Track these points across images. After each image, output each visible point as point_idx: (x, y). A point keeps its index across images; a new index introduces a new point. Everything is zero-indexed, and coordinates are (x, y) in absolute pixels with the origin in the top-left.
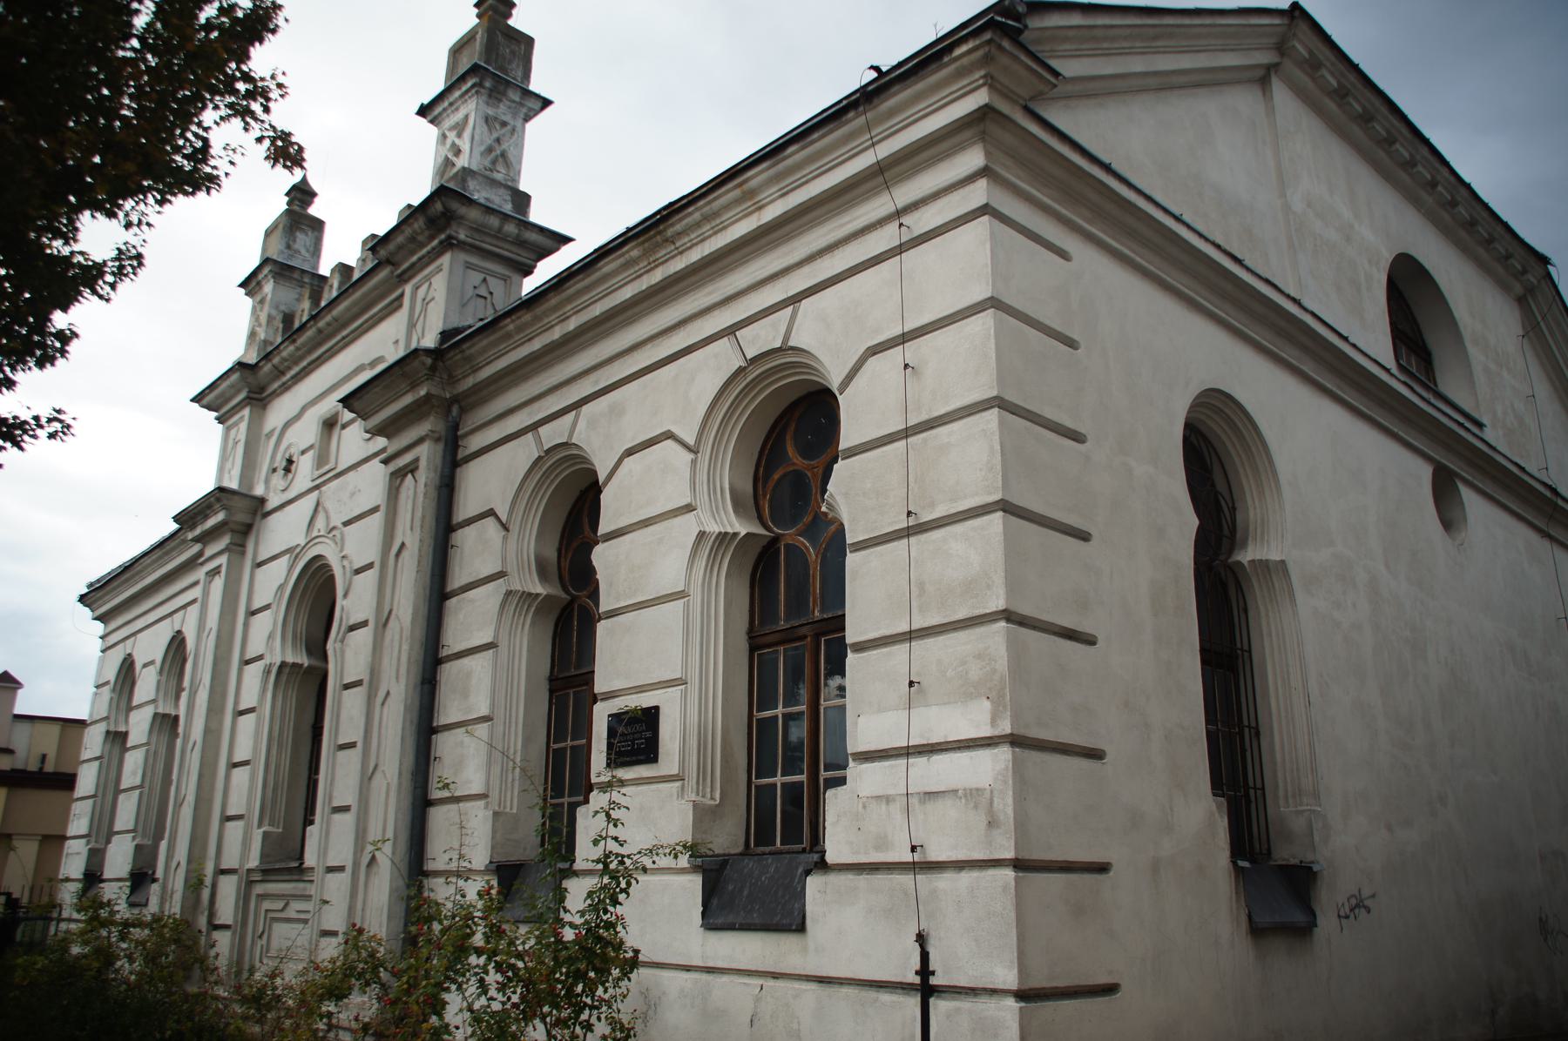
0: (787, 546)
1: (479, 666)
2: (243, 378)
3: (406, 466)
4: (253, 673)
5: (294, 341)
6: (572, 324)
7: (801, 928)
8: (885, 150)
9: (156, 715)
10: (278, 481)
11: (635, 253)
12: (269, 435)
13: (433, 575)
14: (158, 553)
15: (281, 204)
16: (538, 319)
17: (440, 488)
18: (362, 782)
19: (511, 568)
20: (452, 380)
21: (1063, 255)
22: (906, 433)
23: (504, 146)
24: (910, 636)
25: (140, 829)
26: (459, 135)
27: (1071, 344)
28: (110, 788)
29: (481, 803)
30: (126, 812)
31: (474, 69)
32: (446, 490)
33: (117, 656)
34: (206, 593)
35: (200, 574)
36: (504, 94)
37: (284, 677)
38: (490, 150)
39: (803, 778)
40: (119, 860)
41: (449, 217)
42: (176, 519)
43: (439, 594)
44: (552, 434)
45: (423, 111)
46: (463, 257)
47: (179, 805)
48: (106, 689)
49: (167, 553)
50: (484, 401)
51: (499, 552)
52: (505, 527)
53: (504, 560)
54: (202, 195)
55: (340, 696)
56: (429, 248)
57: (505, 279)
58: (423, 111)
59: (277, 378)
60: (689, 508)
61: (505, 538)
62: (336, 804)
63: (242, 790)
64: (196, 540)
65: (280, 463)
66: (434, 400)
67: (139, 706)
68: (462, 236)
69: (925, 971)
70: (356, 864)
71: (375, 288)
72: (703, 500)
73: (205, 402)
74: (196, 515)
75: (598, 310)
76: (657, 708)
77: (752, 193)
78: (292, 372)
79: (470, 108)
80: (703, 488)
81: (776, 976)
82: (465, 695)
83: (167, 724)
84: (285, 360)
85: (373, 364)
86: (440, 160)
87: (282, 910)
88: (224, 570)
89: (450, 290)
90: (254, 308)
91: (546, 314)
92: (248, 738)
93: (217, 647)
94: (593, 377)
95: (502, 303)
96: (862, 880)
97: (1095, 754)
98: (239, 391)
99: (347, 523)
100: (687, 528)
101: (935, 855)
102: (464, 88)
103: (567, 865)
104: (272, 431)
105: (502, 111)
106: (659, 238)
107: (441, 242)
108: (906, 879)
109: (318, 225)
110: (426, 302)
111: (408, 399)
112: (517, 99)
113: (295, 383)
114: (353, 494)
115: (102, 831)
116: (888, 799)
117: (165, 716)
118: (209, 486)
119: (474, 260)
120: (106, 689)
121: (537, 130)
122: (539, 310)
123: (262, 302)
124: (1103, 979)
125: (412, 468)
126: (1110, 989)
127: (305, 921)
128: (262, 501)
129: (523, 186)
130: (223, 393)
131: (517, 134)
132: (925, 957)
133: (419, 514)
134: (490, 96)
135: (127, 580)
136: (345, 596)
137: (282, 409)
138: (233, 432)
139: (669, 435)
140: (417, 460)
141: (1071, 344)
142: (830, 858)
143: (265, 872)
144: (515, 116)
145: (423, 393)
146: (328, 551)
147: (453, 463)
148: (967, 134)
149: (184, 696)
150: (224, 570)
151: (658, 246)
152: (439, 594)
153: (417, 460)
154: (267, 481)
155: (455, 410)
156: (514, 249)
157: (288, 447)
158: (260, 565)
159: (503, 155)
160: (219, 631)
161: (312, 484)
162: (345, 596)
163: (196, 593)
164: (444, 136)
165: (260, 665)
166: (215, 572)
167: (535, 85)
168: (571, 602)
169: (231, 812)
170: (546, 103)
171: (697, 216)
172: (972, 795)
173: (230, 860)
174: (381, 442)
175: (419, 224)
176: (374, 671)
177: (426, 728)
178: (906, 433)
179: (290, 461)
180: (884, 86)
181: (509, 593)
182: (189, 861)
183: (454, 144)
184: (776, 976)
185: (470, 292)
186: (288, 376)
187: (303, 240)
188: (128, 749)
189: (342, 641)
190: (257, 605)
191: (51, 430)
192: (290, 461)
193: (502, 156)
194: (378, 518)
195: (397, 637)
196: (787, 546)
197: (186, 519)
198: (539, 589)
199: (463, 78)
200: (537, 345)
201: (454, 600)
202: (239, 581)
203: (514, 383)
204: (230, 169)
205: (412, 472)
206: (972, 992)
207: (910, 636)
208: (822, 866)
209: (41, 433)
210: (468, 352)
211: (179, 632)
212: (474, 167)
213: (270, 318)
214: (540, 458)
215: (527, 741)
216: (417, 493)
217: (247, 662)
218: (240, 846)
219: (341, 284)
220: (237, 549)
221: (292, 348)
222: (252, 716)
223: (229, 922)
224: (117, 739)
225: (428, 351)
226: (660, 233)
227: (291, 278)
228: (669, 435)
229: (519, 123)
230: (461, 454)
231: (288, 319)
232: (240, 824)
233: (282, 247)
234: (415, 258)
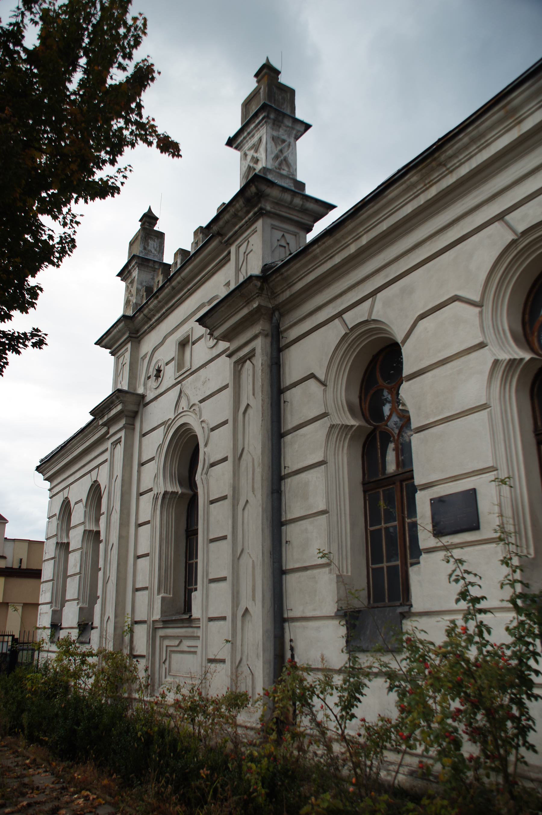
0: (381, 432)
1: (315, 478)
2: (126, 325)
3: (245, 356)
4: (146, 501)
5: (157, 297)
6: (364, 240)
9: (85, 531)
10: (152, 383)
11: (414, 179)
13: (272, 422)
14: (81, 436)
15: (137, 226)
16: (337, 241)
17: (271, 366)
18: (233, 561)
19: (331, 410)
20: (274, 295)
23: (285, 154)
25: (81, 598)
26: (256, 151)
28: (62, 575)
29: (327, 570)
30: (72, 588)
31: (264, 107)
32: (276, 367)
33: (59, 500)
34: (112, 455)
35: (108, 444)
36: (282, 122)
37: (167, 501)
38: (277, 157)
40: (70, 617)
41: (260, 196)
42: (92, 413)
43: (277, 434)
44: (353, 318)
45: (230, 142)
46: (269, 221)
47: (106, 582)
48: (55, 519)
49: (86, 436)
50: (289, 311)
51: (320, 402)
52: (324, 384)
53: (326, 405)
54: (109, 198)
55: (208, 507)
56: (247, 218)
57: (295, 235)
58: (230, 142)
59: (147, 322)
60: (481, 345)
61: (325, 391)
62: (211, 577)
63: (145, 572)
64: (104, 424)
65: (152, 372)
66: (263, 311)
67: (75, 527)
68: (268, 208)
70: (234, 616)
71: (209, 254)
72: (491, 338)
73: (103, 343)
74: (104, 408)
75: (384, 226)
76: (474, 490)
77: (515, 110)
78: (156, 318)
79: (263, 133)
80: (490, 331)
83: (93, 537)
84: (151, 310)
85: (210, 302)
86: (245, 169)
87: (178, 645)
88: (123, 440)
89: (264, 242)
90: (127, 287)
91: (343, 237)
92: (146, 540)
93: (122, 486)
94: (383, 273)
95: (295, 249)
98: (124, 334)
99: (201, 401)
100: (483, 360)
102: (257, 121)
103: (187, 617)
104: (146, 354)
105: (282, 133)
106: (434, 164)
107: (255, 214)
109: (161, 235)
110: (246, 255)
111: (245, 312)
112: (290, 125)
113: (158, 324)
114: (204, 383)
115: (59, 600)
117: (90, 531)
118: (108, 391)
119: (277, 223)
120: (55, 519)
121: (304, 146)
122: (338, 235)
123: (132, 282)
125: (250, 356)
127: (195, 653)
128: (143, 396)
129: (299, 178)
130: (114, 336)
131: (292, 147)
133: (259, 383)
134: (274, 124)
135: (63, 455)
136: (206, 445)
138: (121, 360)
139: (456, 299)
140: (254, 350)
143: (164, 622)
144: (289, 136)
145: (255, 305)
146: (192, 420)
149: (103, 519)
150: (123, 440)
151: (433, 170)
152: (277, 434)
153: (254, 350)
154: (145, 385)
155: (277, 314)
156: (300, 215)
157: (157, 362)
158: (144, 435)
159: (285, 159)
160: (123, 476)
161: (175, 382)
162: (206, 445)
163: (106, 456)
164: (246, 155)
165: (150, 495)
166: (118, 441)
167: (299, 115)
168: (374, 431)
169: (138, 586)
170: (308, 127)
171: (466, 140)
174: (223, 345)
175: (241, 202)
176: (235, 489)
177: (277, 522)
179: (159, 371)
181: (332, 427)
182: (116, 617)
183: (253, 157)
185: (276, 244)
186: (154, 320)
187: (152, 244)
188: (70, 552)
189: (207, 474)
190: (144, 459)
191: (34, 341)
192: (159, 371)
193: (285, 161)
194: (228, 392)
195: (250, 465)
196: (381, 432)
197: (98, 412)
199: (256, 115)
200: (337, 259)
201: (289, 437)
202: (132, 445)
203: (320, 290)
204: (124, 180)
205: (249, 359)
209: (29, 343)
210: (285, 274)
211: (67, 498)
212: (269, 167)
213: (138, 290)
214: (346, 334)
215: (353, 525)
216: (255, 372)
217: (142, 494)
218: (148, 606)
219: (182, 260)
220: (130, 427)
221: (156, 302)
222: (148, 526)
223: (144, 653)
224: (64, 547)
225: (257, 277)
226: (435, 159)
227: (148, 266)
228: (456, 299)
229: (292, 140)
230: (283, 343)
231: (149, 290)
232: (146, 592)
233: (141, 249)
234: (237, 227)
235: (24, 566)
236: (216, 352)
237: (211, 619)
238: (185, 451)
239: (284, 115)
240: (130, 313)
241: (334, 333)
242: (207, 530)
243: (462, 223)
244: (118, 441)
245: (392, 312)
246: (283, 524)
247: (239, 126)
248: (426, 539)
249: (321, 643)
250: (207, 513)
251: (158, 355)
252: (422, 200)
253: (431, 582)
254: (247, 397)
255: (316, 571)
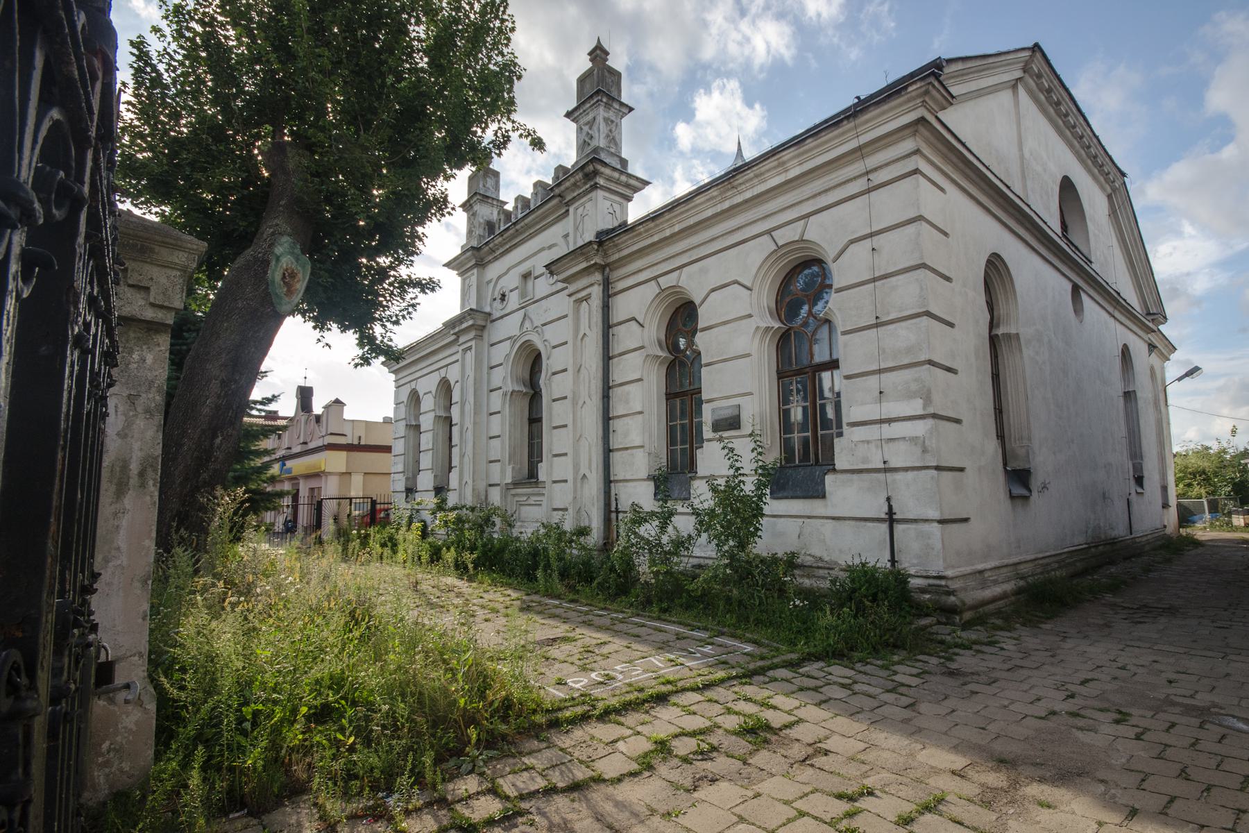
7: (824, 497)
8: (864, 139)
10: (497, 304)
12: (490, 281)
16: (657, 226)
20: (606, 255)
21: (942, 190)
22: (874, 280)
24: (880, 371)
27: (946, 234)
32: (606, 308)
33: (406, 391)
34: (463, 359)
39: (809, 434)
45: (568, 115)
51: (641, 337)
58: (568, 115)
60: (750, 316)
65: (497, 295)
69: (891, 512)
70: (575, 479)
75: (692, 221)
81: (809, 517)
82: (627, 402)
90: (469, 219)
96: (855, 476)
97: (958, 421)
100: (751, 324)
101: (892, 464)
108: (881, 476)
111: (584, 265)
116: (868, 442)
119: (607, 195)
124: (965, 516)
126: (966, 520)
129: (623, 156)
132: (890, 507)
137: (494, 270)
141: (946, 234)
142: (838, 467)
147: (608, 296)
148: (907, 132)
151: (728, 190)
159: (614, 138)
165: (501, 391)
166: (470, 348)
167: (624, 99)
170: (631, 109)
172: (914, 440)
173: (496, 479)
178: (874, 280)
179: (503, 296)
180: (861, 107)
184: (809, 517)
187: (490, 182)
192: (503, 296)
198: (660, 353)
206: (915, 521)
207: (880, 371)
208: (834, 470)
215: (659, 421)
220: (479, 337)
232: (498, 464)
235: (363, 443)
236: (555, 288)
237: (555, 482)
238: (532, 362)
239: (614, 99)
240: (475, 243)
241: (651, 290)
242: (550, 420)
243: (744, 230)
244: (470, 348)
245: (694, 283)
246: (610, 419)
247: (575, 105)
248: (707, 433)
249: (640, 494)
250: (550, 409)
251: (502, 282)
252: (719, 208)
253: (712, 460)
254: (584, 327)
255: (634, 451)
